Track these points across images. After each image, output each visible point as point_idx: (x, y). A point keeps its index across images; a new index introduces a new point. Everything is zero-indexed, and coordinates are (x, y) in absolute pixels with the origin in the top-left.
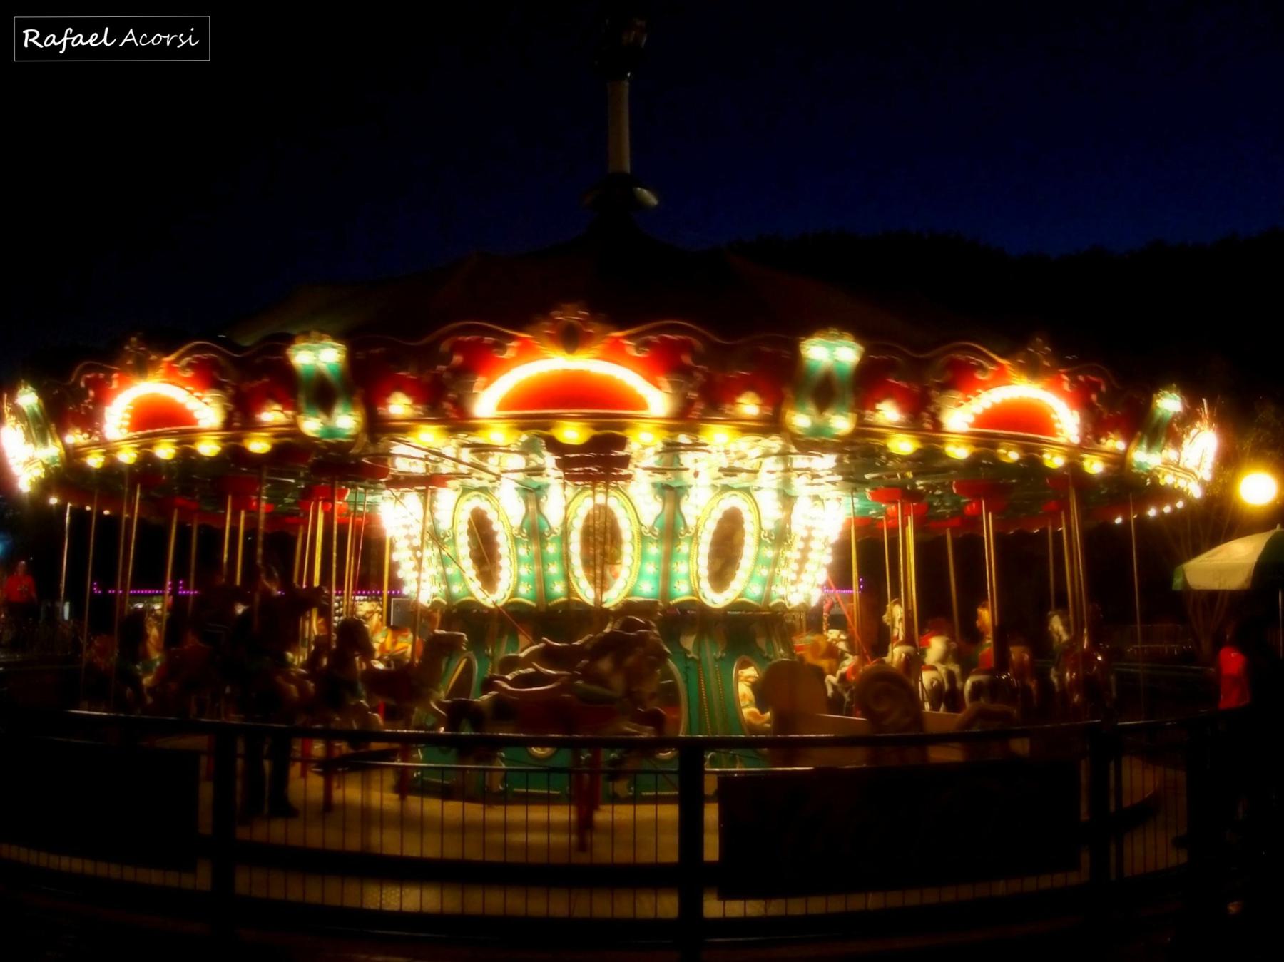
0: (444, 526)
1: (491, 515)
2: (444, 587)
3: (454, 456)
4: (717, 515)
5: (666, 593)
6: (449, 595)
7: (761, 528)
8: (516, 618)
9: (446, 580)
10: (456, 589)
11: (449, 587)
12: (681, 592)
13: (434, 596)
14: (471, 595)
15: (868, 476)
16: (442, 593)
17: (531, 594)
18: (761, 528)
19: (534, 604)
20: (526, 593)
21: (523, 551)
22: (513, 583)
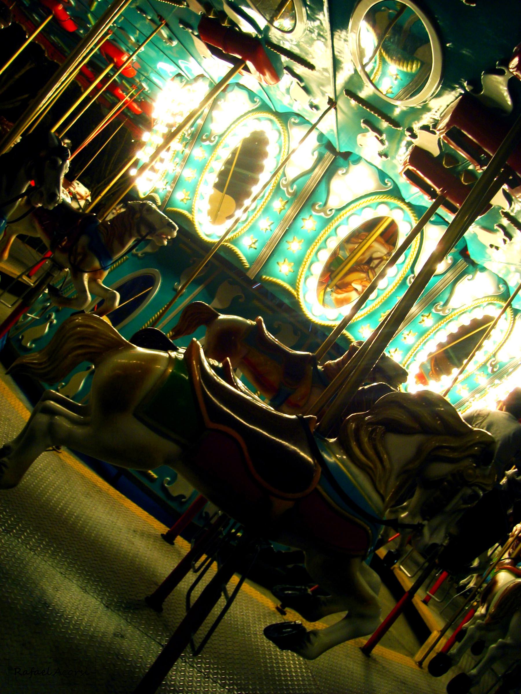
0: (215, 127)
1: (271, 149)
2: (169, 189)
3: (317, 126)
4: (479, 315)
5: (265, 262)
6: (167, 202)
7: (494, 355)
8: (221, 270)
9: (177, 182)
10: (180, 196)
11: (174, 189)
12: (281, 272)
13: (155, 191)
14: (191, 212)
15: (338, 456)
16: (162, 192)
17: (251, 252)
18: (494, 355)
19: (247, 265)
20: (246, 249)
21: (278, 204)
22: (241, 231)
